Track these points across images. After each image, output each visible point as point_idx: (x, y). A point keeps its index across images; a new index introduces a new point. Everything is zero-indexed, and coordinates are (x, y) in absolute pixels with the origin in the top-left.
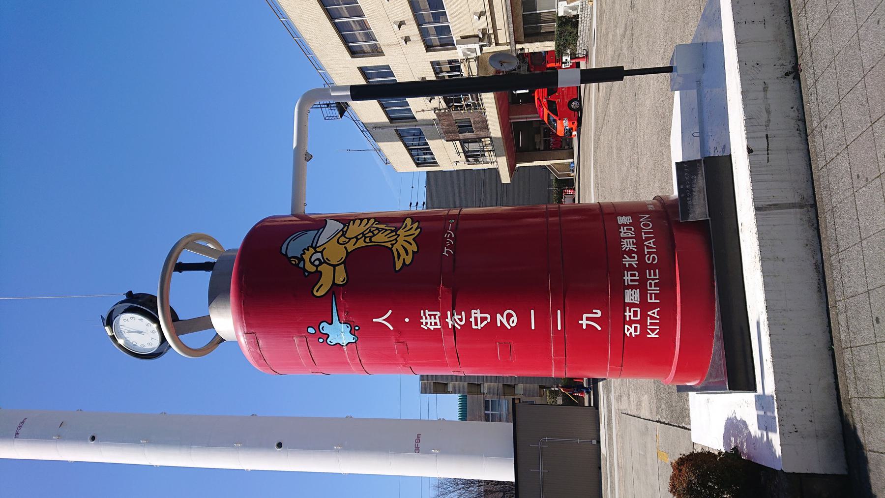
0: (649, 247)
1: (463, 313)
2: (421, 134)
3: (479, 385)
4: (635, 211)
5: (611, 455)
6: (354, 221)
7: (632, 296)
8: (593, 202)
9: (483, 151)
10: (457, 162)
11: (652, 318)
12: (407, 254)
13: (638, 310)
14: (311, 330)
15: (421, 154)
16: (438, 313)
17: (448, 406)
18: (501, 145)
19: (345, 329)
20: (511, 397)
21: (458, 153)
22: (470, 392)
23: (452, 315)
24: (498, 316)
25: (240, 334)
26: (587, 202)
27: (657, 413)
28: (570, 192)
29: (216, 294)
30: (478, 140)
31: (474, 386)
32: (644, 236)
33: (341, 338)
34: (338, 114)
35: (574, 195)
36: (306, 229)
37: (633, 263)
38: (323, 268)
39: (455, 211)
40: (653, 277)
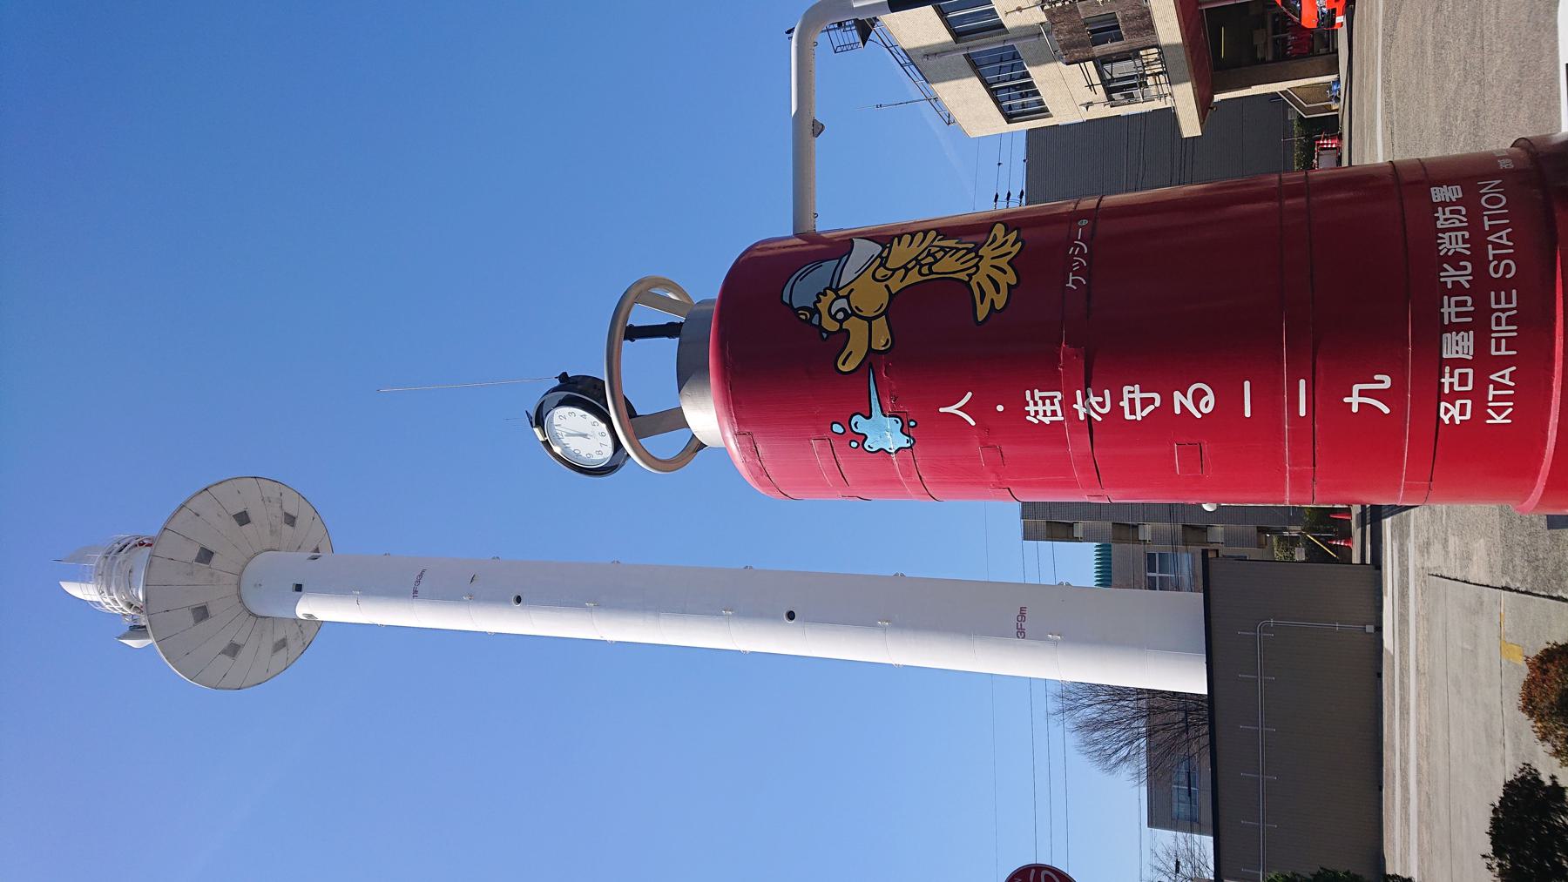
0: (1496, 246)
1: (1107, 392)
2: (1015, 56)
3: (1136, 527)
4: (1469, 174)
5: (1403, 653)
6: (900, 237)
7: (1458, 346)
8: (1380, 160)
9: (1144, 75)
10: (1088, 105)
11: (1498, 386)
12: (998, 291)
13: (1470, 371)
14: (837, 428)
15: (1014, 96)
16: (1059, 395)
17: (1077, 561)
18: (1182, 61)
19: (892, 424)
20: (1199, 549)
21: (1091, 86)
22: (1118, 540)
23: (1086, 397)
24: (1177, 395)
25: (729, 435)
26: (1367, 162)
27: (1504, 573)
28: (1331, 143)
29: (688, 373)
30: (1132, 54)
31: (1125, 530)
32: (1487, 223)
33: (887, 441)
34: (858, 39)
35: (1338, 149)
36: (818, 259)
37: (1462, 280)
38: (852, 324)
39: (1089, 203)
40: (1505, 305)
